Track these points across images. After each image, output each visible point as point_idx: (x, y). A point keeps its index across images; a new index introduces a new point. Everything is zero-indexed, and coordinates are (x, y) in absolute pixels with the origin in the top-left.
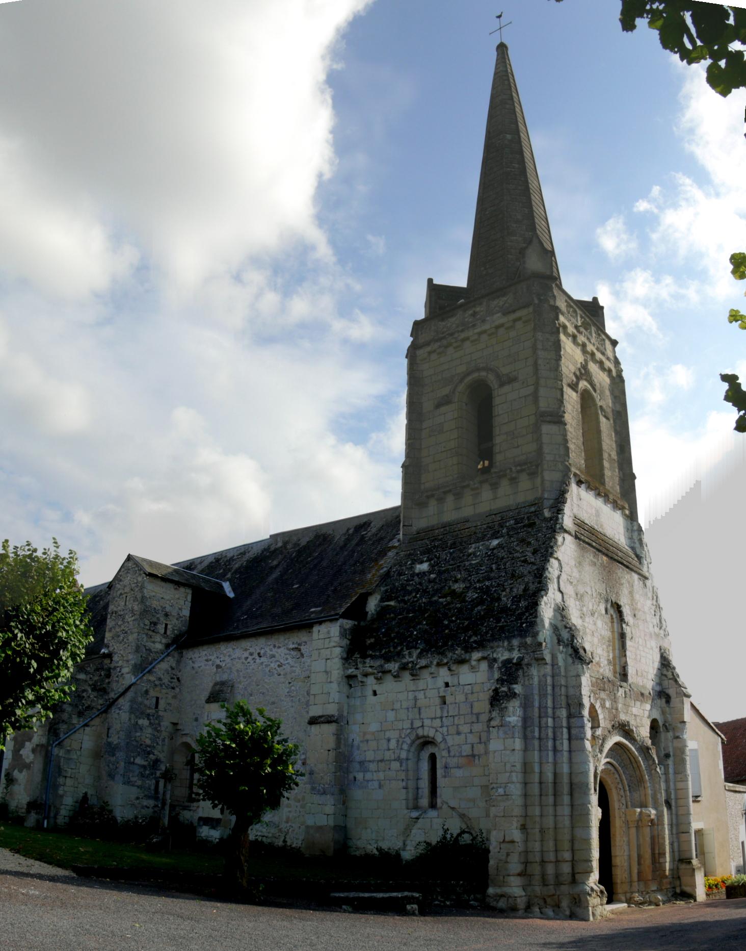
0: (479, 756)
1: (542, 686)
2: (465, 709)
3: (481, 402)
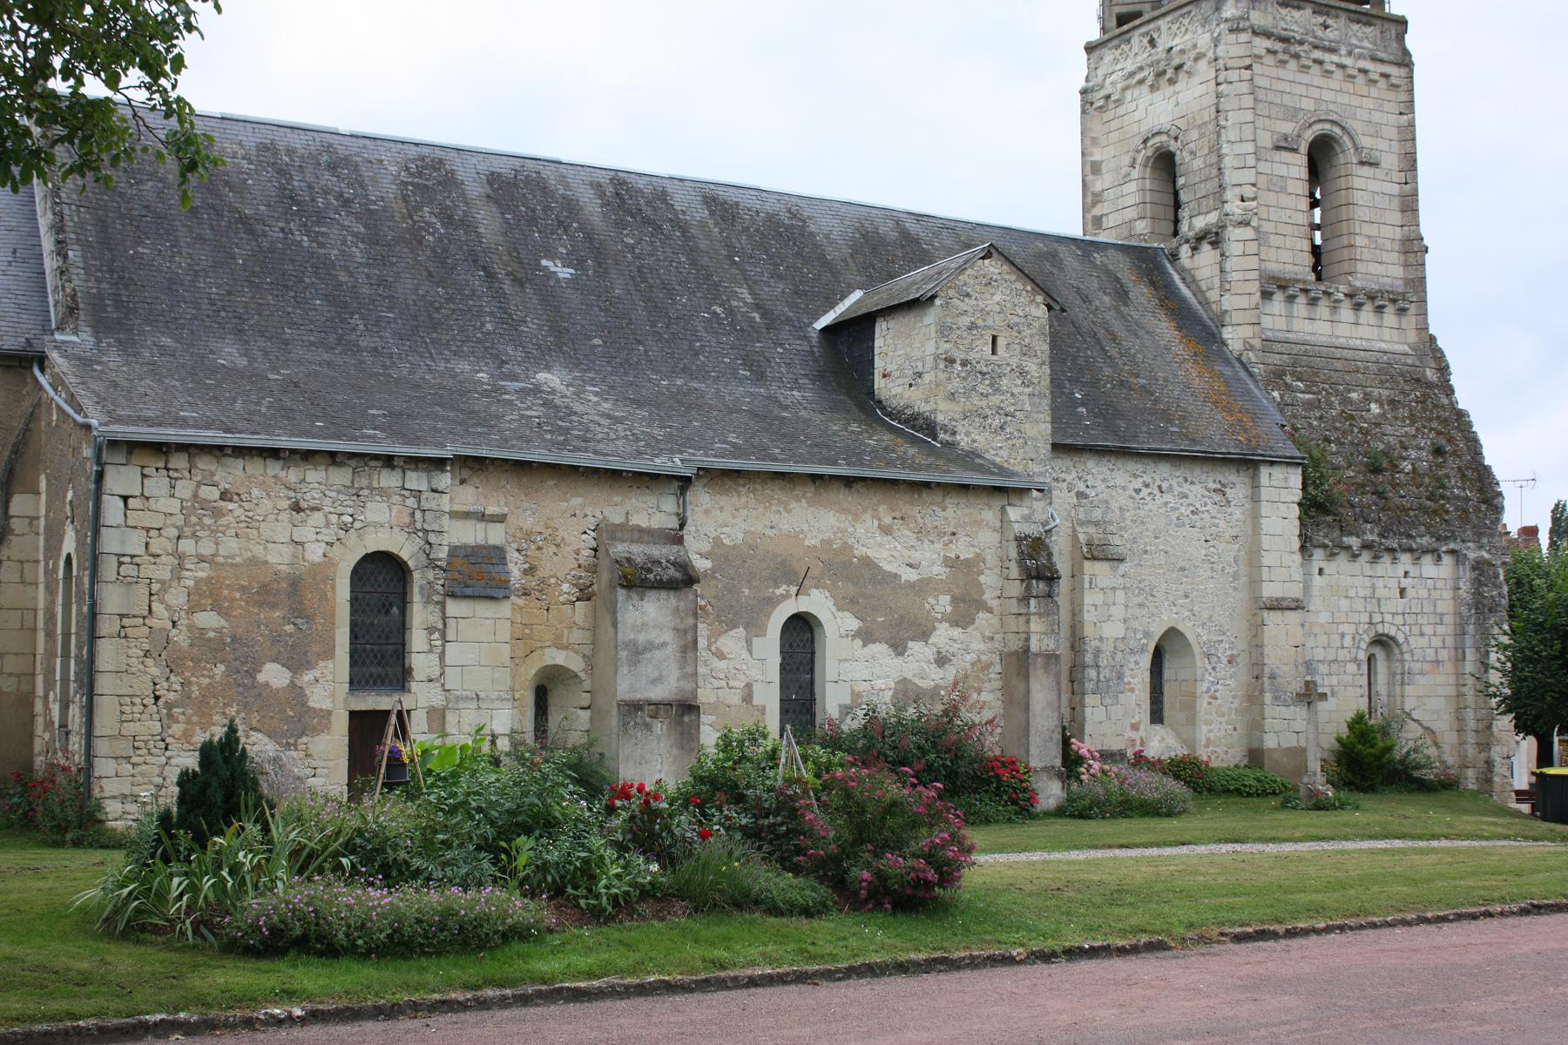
2: (1428, 608)
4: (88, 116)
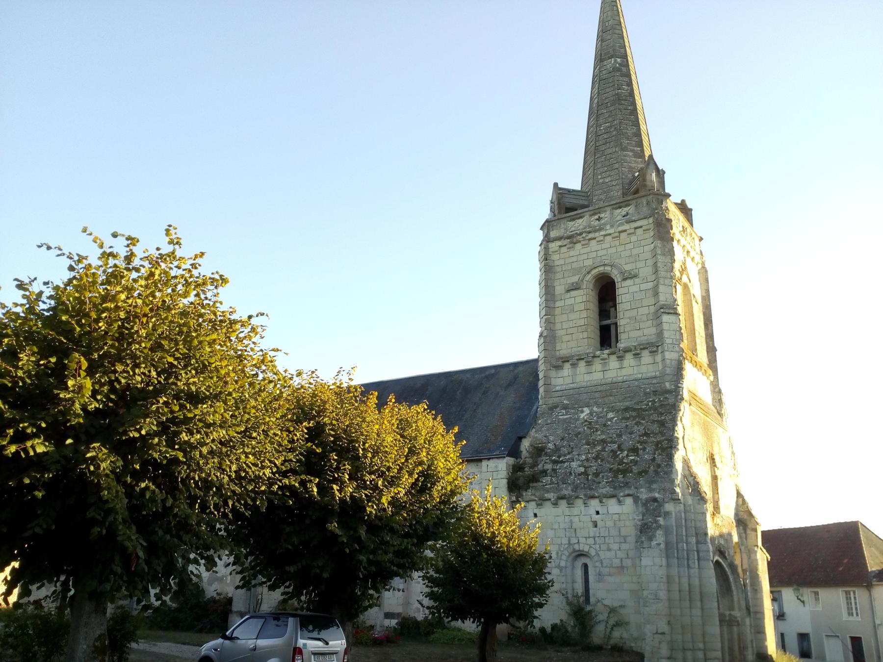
1: (678, 520)
2: (614, 532)
3: (606, 292)
4: (663, 450)
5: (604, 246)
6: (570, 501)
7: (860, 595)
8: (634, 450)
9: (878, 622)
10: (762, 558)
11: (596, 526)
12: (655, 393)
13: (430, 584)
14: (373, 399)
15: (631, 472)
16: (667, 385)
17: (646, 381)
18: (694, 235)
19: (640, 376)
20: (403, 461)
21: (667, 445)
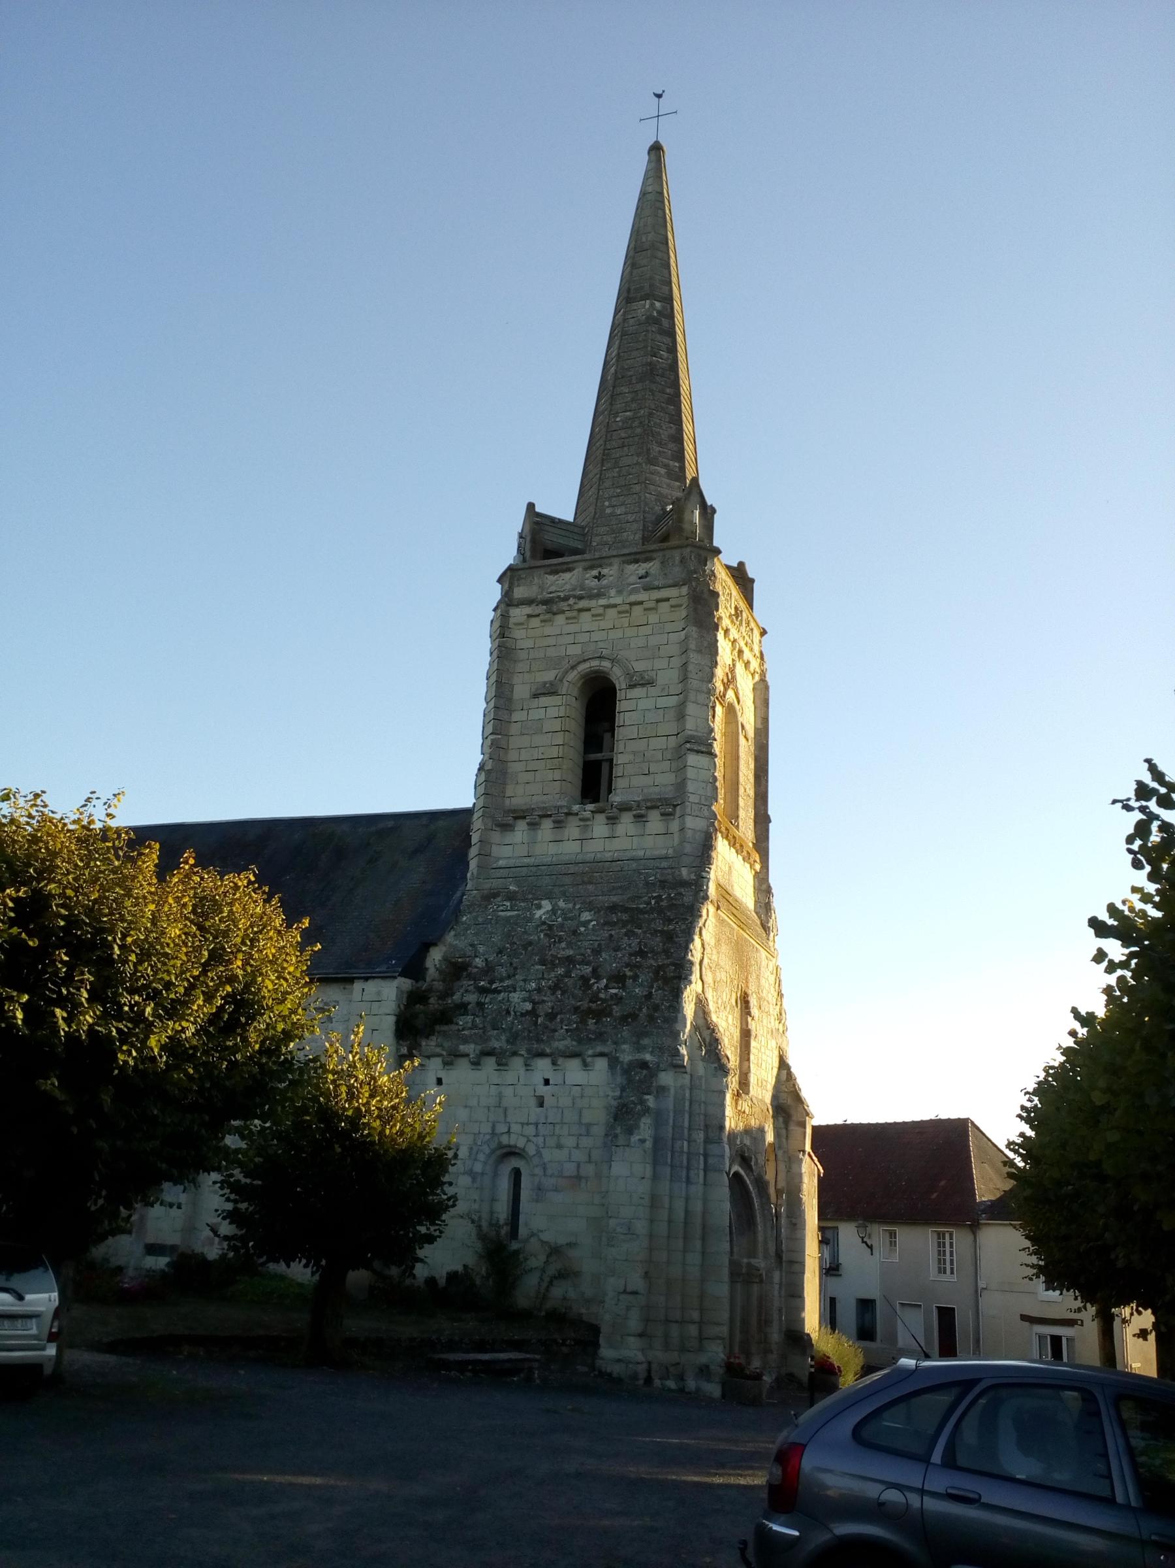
0: (587, 1179)
3: (599, 703)
4: (666, 980)
5: (603, 624)
6: (502, 1059)
7: (959, 1239)
8: (618, 979)
9: (981, 1284)
10: (810, 1171)
11: (541, 1105)
12: (663, 884)
13: (233, 1196)
14: (151, 856)
15: (610, 1015)
16: (684, 872)
17: (652, 863)
18: (752, 625)
19: (641, 853)
20: (196, 973)
21: (675, 972)
